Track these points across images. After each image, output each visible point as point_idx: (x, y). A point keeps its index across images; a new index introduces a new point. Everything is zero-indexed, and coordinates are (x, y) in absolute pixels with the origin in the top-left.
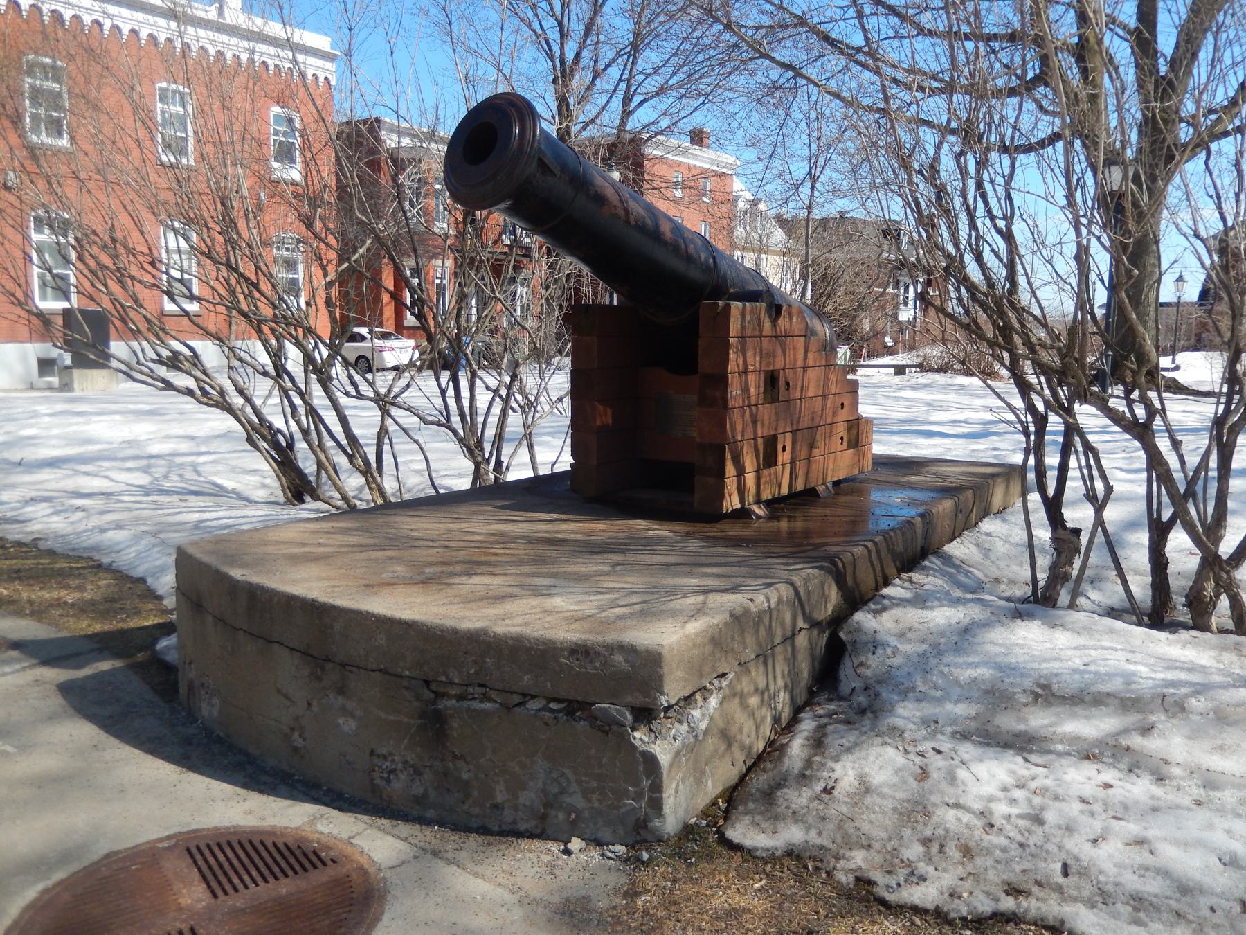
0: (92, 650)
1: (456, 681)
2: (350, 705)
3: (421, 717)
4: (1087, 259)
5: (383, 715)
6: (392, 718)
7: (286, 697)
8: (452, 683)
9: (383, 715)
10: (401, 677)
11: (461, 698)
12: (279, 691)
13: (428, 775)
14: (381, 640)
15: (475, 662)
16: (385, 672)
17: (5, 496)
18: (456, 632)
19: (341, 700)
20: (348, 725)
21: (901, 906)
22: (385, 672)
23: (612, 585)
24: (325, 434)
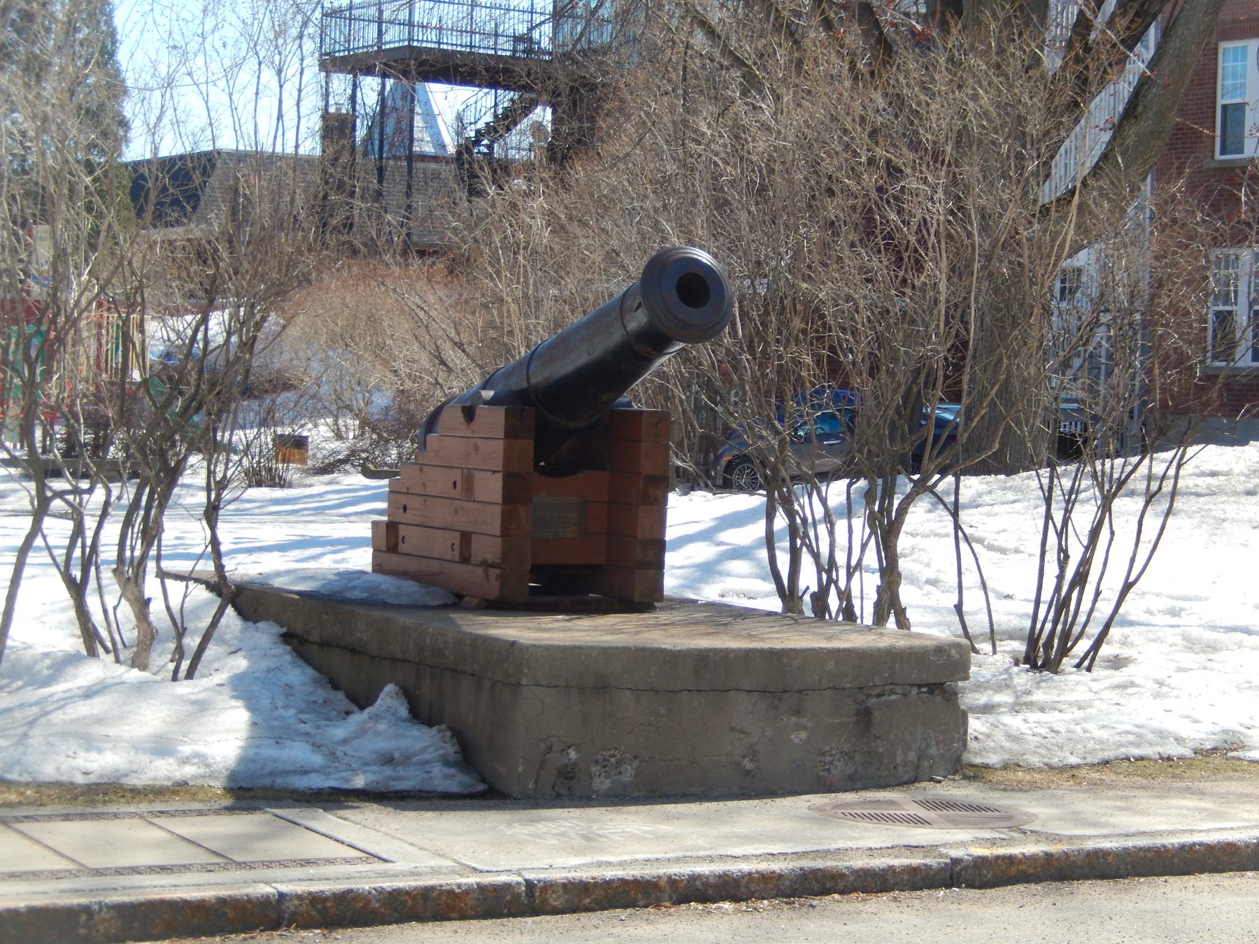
0: (127, 775)
1: (878, 683)
2: (804, 721)
3: (857, 715)
4: (155, 536)
5: (830, 721)
6: (837, 721)
7: (741, 731)
8: (875, 686)
9: (830, 721)
10: (844, 689)
11: (878, 696)
12: (733, 729)
13: (858, 757)
14: (831, 665)
15: (890, 668)
16: (834, 688)
17: (1257, 480)
18: (879, 650)
19: (794, 719)
20: (799, 737)
21: (274, 800)
22: (834, 688)
23: (581, 634)
24: (1107, 520)
